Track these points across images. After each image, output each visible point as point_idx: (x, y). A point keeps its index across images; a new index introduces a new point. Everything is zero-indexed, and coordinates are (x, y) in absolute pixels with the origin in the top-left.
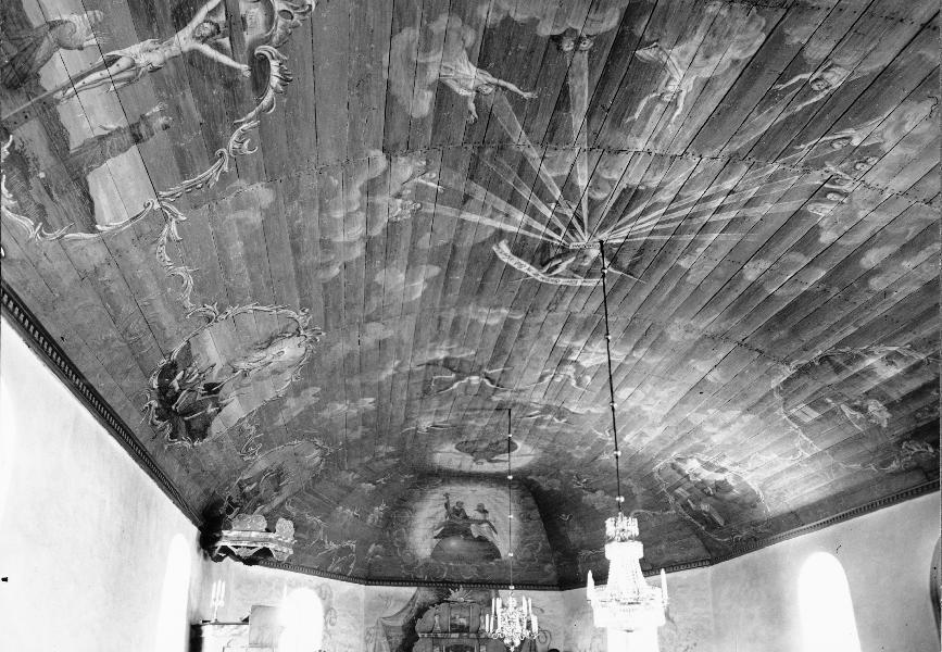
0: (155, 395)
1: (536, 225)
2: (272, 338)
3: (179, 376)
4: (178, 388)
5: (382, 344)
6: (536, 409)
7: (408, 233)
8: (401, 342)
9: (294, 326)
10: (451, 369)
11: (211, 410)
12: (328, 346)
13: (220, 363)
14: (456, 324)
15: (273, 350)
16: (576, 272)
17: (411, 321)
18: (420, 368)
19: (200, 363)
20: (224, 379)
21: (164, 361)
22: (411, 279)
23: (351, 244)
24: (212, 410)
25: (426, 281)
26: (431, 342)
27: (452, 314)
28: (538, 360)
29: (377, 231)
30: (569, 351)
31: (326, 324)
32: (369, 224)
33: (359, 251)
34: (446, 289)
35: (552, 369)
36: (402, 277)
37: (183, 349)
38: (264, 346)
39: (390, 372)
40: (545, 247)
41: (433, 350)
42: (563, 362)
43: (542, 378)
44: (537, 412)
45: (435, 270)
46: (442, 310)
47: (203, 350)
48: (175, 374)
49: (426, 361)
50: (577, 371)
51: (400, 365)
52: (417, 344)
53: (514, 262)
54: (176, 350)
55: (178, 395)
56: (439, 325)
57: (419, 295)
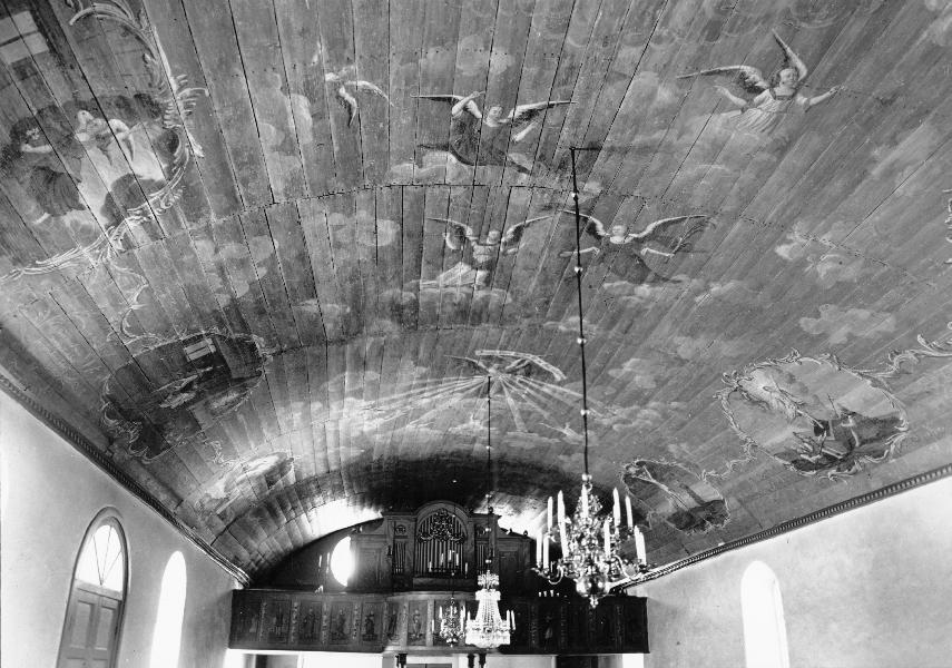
0: (824, 472)
1: (536, 386)
2: (754, 403)
3: (806, 457)
5: (693, 333)
7: (618, 399)
8: (676, 323)
9: (733, 395)
10: (642, 263)
11: (851, 422)
12: (735, 361)
13: (791, 429)
14: (613, 322)
15: (766, 395)
16: (501, 360)
17: (652, 341)
18: (679, 277)
19: (794, 445)
20: (809, 420)
21: (792, 468)
22: (631, 375)
23: (655, 409)
24: (851, 421)
26: (647, 310)
27: (612, 333)
28: (526, 268)
29: (635, 407)
30: (488, 281)
31: (715, 378)
32: (636, 411)
33: (653, 404)
34: (608, 358)
35: (504, 254)
36: (637, 378)
38: (764, 405)
39: (715, 288)
40: (528, 374)
41: (650, 300)
42: (490, 266)
43: (518, 232)
44: (519, 136)
45: (612, 372)
46: (619, 341)
47: (781, 444)
48: (803, 460)
49: (667, 284)
50: (471, 254)
51: (698, 293)
52: (662, 311)
53: (551, 368)
54: (781, 462)
56: (629, 327)
57: (633, 360)
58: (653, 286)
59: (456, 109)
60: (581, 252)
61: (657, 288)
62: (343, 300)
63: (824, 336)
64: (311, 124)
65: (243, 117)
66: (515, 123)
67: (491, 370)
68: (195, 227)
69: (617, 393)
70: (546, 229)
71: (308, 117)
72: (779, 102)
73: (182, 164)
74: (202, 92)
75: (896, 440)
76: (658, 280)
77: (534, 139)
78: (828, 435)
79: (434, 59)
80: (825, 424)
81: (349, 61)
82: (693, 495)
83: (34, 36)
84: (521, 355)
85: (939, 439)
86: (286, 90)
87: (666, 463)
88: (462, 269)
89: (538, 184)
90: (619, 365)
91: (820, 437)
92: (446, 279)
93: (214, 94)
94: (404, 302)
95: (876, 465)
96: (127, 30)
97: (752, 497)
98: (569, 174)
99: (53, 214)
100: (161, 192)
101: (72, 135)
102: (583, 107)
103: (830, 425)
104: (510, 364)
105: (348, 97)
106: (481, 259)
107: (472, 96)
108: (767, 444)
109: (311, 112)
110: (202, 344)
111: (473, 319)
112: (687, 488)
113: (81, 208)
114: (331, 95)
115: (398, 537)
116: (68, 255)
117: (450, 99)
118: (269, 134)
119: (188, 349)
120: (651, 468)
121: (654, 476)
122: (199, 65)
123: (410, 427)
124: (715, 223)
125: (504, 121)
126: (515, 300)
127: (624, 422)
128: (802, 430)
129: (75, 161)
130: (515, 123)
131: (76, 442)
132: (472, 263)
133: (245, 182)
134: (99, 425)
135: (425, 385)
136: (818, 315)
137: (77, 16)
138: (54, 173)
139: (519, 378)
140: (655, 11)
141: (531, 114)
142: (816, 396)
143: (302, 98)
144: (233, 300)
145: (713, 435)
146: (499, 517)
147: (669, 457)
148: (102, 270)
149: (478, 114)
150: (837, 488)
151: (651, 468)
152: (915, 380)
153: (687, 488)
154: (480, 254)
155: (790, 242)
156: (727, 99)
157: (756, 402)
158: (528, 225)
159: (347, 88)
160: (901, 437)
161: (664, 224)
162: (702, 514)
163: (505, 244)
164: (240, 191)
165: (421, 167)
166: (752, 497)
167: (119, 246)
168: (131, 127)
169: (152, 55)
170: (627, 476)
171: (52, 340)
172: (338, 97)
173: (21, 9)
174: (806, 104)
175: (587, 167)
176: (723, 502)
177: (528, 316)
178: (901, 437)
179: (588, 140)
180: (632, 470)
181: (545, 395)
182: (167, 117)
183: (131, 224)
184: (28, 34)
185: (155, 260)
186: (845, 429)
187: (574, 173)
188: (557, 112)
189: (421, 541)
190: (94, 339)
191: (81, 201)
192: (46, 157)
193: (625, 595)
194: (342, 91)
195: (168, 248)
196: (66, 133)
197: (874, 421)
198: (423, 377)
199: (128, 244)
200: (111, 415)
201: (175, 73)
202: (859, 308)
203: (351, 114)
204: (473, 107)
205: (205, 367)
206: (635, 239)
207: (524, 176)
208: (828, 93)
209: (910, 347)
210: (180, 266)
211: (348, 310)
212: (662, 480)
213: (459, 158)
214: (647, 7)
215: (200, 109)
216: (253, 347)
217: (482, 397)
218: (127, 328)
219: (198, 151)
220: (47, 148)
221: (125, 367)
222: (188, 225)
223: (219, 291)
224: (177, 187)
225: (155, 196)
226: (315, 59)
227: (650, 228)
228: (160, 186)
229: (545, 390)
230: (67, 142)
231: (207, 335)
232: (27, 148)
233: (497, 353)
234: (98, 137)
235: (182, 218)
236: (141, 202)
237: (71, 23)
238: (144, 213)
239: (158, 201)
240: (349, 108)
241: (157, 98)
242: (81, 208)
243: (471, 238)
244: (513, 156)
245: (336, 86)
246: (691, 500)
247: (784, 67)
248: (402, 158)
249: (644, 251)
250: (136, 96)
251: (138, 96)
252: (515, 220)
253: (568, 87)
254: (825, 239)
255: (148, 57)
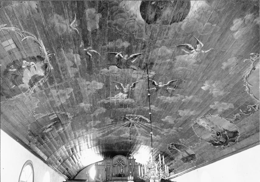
3: (215, 142)
4: (219, 142)
6: (134, 64)
9: (195, 125)
11: (226, 133)
13: (211, 134)
15: (203, 125)
19: (212, 139)
20: (215, 132)
21: (212, 145)
25: (165, 118)
26: (170, 103)
30: (128, 97)
33: (174, 128)
37: (209, 142)
38: (203, 128)
40: (140, 121)
44: (133, 61)
46: (164, 111)
47: (208, 139)
48: (215, 143)
54: (209, 143)
55: (221, 142)
58: (171, 97)
59: (117, 56)
60: (150, 89)
61: (172, 98)
62: (90, 103)
63: (216, 110)
64: (80, 61)
65: (64, 60)
66: (132, 59)
67: (130, 120)
68: (52, 86)
69: (164, 125)
70: (141, 84)
71: (80, 59)
72: (197, 52)
73: (48, 71)
74: (53, 55)
75: (238, 137)
76: (171, 96)
77: (137, 62)
78: (221, 136)
79: (111, 45)
80: (219, 133)
81: (89, 46)
82: (187, 153)
83: (13, 44)
84: (138, 115)
85: (249, 137)
86: (74, 53)
87: (179, 144)
88: (121, 94)
89: (139, 73)
90: (164, 118)
91: (218, 137)
92: (117, 97)
93: (56, 55)
94: (106, 103)
95: (233, 144)
96: (35, 42)
97: (202, 153)
98: (146, 70)
99: (16, 85)
100: (43, 78)
101: (21, 66)
102: (50, 96)
103: (221, 133)
104: (135, 118)
105: (89, 54)
106: (126, 91)
107: (120, 53)
108: (205, 138)
109: (80, 57)
110: (54, 115)
111: (124, 107)
112: (185, 151)
113: (23, 83)
114: (85, 54)
115: (108, 166)
116: (20, 95)
117: (114, 54)
118: (68, 63)
119: (50, 117)
120: (175, 145)
121: (176, 148)
122: (52, 48)
123: (110, 135)
124: (185, 81)
125: (129, 58)
126: (135, 101)
127: (167, 133)
128: (214, 135)
129: (22, 72)
130: (132, 59)
131: (19, 142)
132: (123, 92)
133: (64, 75)
134: (27, 138)
135: (113, 124)
136: (214, 104)
137: (23, 39)
138: (17, 75)
139: (138, 121)
140: (164, 32)
141: (135, 56)
142: (216, 126)
143: (78, 54)
144: (62, 104)
145: (191, 136)
146: (135, 159)
147: (179, 142)
148: (28, 98)
149: (122, 57)
150: (224, 150)
151: (175, 145)
152: (241, 121)
153: (185, 151)
154: (125, 90)
155: (205, 86)
156: (185, 52)
157: (201, 127)
158: (137, 83)
159: (89, 52)
160: (239, 136)
161: (172, 82)
162: (190, 158)
163: (131, 87)
164: (63, 77)
165: (108, 69)
166: (202, 153)
167: (33, 92)
168: (36, 64)
169: (41, 47)
170: (169, 147)
171: (15, 116)
172: (87, 54)
173: (10, 39)
174: (204, 52)
175: (150, 68)
176: (195, 155)
177: (139, 106)
178: (239, 136)
179: (151, 62)
180: (170, 146)
181: (145, 126)
182: (45, 61)
183: (35, 87)
184: (11, 44)
185: (41, 95)
186: (225, 134)
187: (147, 71)
188: (142, 56)
189: (114, 166)
190: (26, 116)
191: (23, 82)
192: (15, 72)
193: (170, 181)
194: (88, 53)
195: (45, 92)
196: (20, 66)
197: (232, 132)
198: (112, 122)
199: (35, 91)
200: (30, 135)
201: (47, 51)
202: (224, 102)
203: (90, 58)
204: (121, 55)
205: (55, 121)
206: (165, 86)
207: (135, 71)
208: (209, 50)
209: (238, 112)
210: (48, 96)
211: (92, 105)
212: (178, 149)
213: (118, 67)
214: (162, 31)
215: (52, 59)
216: (67, 116)
217: (129, 127)
218: (35, 113)
219: (52, 68)
220: (15, 70)
221: (34, 122)
222: (50, 86)
223: (58, 102)
224: (47, 77)
225: (42, 79)
226: (81, 46)
227: (169, 83)
228: (43, 77)
229: (145, 124)
230: (20, 68)
231: (55, 113)
232: (10, 70)
233: (131, 115)
234: (28, 66)
235: (48, 84)
236: (38, 81)
237: (22, 41)
238: (39, 84)
239: (42, 80)
240: (90, 56)
241: (42, 57)
242: (23, 83)
243: (123, 86)
244: (132, 66)
245: (86, 52)
246: (187, 154)
247: (197, 44)
248: (103, 67)
249: (168, 88)
250: (37, 56)
251: (38, 56)
252: (133, 82)
253: (144, 50)
254: (214, 85)
255: (40, 47)
